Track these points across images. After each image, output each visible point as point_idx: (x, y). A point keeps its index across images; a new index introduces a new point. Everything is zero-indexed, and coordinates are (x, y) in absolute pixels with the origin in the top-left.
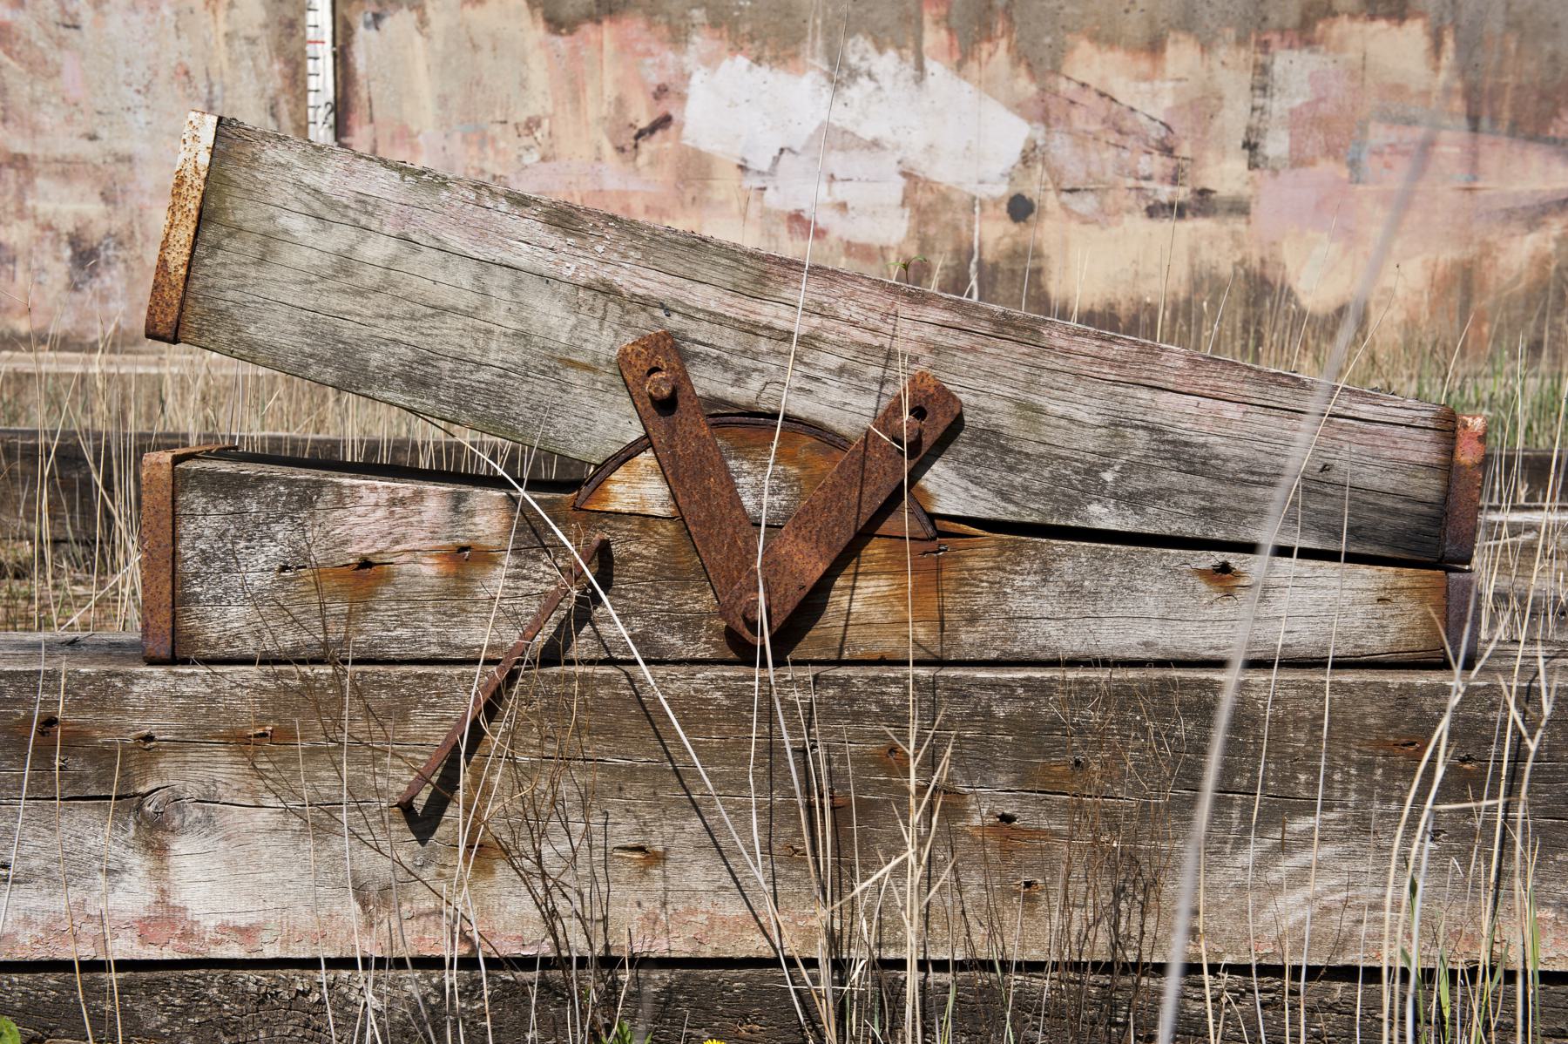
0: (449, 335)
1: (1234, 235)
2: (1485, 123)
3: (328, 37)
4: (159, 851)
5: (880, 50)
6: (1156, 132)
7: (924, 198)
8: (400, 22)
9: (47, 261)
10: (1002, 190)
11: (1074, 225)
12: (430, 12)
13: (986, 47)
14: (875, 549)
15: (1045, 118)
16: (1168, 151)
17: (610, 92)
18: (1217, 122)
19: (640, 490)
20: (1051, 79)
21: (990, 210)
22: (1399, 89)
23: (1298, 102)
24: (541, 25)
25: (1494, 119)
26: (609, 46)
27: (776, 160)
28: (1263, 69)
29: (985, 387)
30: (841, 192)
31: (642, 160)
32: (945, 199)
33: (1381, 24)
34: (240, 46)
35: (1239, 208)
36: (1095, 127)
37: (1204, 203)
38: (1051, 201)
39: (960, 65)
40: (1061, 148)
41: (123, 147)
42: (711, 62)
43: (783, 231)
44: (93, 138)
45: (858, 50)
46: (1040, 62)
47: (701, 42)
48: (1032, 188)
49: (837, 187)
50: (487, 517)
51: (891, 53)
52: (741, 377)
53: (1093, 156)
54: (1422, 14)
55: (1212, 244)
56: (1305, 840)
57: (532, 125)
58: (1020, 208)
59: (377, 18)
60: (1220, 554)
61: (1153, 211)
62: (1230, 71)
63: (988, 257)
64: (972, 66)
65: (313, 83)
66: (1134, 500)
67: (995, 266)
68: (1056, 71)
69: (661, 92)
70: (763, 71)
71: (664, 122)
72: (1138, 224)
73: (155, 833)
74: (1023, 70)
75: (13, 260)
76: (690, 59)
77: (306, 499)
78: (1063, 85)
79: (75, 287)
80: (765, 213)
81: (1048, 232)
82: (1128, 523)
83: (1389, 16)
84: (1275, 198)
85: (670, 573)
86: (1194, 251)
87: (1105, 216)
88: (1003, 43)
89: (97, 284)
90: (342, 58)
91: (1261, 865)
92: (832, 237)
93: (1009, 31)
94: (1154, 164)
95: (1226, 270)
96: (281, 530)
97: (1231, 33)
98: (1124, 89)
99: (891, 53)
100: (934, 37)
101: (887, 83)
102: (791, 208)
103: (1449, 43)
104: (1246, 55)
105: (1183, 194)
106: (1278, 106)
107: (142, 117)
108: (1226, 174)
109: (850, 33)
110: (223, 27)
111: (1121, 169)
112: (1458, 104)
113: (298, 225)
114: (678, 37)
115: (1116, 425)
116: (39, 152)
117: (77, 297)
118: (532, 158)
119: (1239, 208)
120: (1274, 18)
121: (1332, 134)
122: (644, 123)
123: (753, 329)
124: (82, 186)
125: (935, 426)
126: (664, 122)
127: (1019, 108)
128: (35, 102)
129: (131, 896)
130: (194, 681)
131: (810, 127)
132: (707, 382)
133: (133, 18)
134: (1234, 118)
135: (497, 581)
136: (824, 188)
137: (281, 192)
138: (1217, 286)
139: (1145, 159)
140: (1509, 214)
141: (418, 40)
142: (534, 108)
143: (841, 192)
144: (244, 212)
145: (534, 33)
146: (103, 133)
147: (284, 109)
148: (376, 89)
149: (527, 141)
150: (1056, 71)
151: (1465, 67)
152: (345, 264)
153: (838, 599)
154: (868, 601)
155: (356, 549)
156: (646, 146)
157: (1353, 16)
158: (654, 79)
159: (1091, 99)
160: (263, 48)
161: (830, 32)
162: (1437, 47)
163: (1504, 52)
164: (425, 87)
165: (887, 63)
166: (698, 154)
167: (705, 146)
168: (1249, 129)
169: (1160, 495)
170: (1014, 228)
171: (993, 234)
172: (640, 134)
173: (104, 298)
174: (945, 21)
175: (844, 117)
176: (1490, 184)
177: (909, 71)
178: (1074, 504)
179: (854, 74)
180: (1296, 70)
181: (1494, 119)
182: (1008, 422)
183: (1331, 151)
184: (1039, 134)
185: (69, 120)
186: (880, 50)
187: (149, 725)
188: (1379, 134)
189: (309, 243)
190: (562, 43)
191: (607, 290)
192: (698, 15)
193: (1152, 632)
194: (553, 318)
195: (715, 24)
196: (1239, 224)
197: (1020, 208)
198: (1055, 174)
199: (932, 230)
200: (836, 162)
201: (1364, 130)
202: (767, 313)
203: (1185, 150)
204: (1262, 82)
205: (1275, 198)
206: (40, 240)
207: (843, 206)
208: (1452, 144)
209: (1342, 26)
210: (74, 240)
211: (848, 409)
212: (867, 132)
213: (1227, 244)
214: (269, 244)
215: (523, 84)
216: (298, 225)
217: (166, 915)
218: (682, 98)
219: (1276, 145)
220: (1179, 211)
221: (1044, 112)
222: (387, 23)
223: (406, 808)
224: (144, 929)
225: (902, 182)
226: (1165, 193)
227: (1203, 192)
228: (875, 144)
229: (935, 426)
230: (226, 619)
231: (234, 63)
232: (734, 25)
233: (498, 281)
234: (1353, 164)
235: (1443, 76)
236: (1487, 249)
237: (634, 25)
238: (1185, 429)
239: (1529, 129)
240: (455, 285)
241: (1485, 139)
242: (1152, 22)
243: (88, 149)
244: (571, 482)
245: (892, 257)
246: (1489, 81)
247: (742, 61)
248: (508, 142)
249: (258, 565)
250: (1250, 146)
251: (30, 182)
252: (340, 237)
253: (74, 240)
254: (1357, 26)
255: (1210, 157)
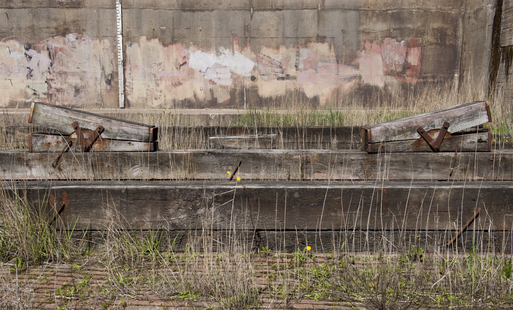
0: (56, 122)
1: (294, 83)
2: (340, 62)
3: (122, 49)
4: (31, 170)
5: (226, 49)
6: (278, 64)
7: (235, 77)
8: (135, 45)
9: (70, 91)
10: (250, 75)
11: (264, 81)
12: (141, 43)
13: (246, 48)
14: (97, 141)
15: (257, 61)
16: (281, 67)
17: (175, 57)
18: (290, 62)
19: (74, 136)
20: (258, 54)
21: (247, 79)
22: (323, 56)
23: (305, 58)
24: (162, 45)
25: (341, 61)
26: (174, 49)
27: (206, 70)
28: (298, 52)
29: (106, 126)
30: (219, 76)
31: (181, 70)
32: (239, 77)
33: (320, 44)
34: (105, 50)
35: (295, 78)
36: (267, 63)
37: (288, 77)
38: (259, 77)
39: (241, 52)
40: (261, 67)
41: (84, 70)
42: (194, 52)
43: (208, 83)
44: (78, 68)
45: (221, 49)
46: (256, 51)
47: (192, 48)
48: (256, 74)
49: (218, 75)
50: (60, 138)
51: (228, 49)
52: (83, 126)
53: (267, 69)
54: (327, 42)
55: (289, 84)
56: (136, 168)
57: (160, 64)
58: (253, 78)
59: (131, 44)
60: (129, 141)
61: (278, 79)
62: (292, 52)
63: (247, 88)
64: (243, 52)
65: (119, 57)
66: (121, 136)
67: (249, 89)
68: (259, 53)
69: (184, 57)
70: (204, 53)
71: (185, 63)
72: (276, 81)
73: (30, 168)
74: (253, 52)
75: (64, 91)
76: (190, 51)
77: (44, 137)
78: (261, 55)
79: (75, 96)
80: (205, 80)
81: (259, 83)
82: (120, 139)
83: (321, 42)
84: (300, 76)
85: (77, 144)
86: (286, 86)
87: (269, 80)
88: (249, 47)
89: (79, 95)
90: (124, 52)
91: (132, 170)
92: (218, 84)
93: (250, 45)
94: (279, 70)
95: (293, 90)
96: (41, 140)
97: (292, 45)
98: (272, 56)
99: (228, 49)
100: (236, 47)
101: (227, 55)
102: (210, 79)
103: (333, 47)
104: (295, 49)
105: (284, 75)
106: (301, 59)
107: (87, 64)
108: (292, 72)
109: (220, 46)
110: (102, 47)
111: (272, 71)
112: (335, 58)
113: (42, 112)
114: (188, 47)
115: (119, 130)
116: (69, 71)
117: (76, 98)
118: (160, 70)
119: (295, 78)
120: (300, 42)
121: (312, 64)
122: (181, 63)
123: (84, 121)
124: (76, 77)
125: (101, 130)
126: (185, 63)
127: (252, 59)
128: (68, 62)
129: (29, 174)
130: (33, 154)
131: (213, 63)
132: (80, 126)
133: (86, 46)
134: (293, 61)
135: (61, 145)
136: (216, 75)
137: (40, 109)
138: (291, 94)
139: (276, 69)
140: (345, 79)
141: (139, 48)
142: (161, 61)
143: (219, 76)
144: (37, 111)
145: (160, 47)
146: (80, 67)
147: (114, 62)
148: (131, 58)
149: (159, 67)
150: (259, 53)
151: (336, 52)
152: (46, 116)
153: (93, 146)
154: (96, 146)
155: (48, 142)
156: (182, 68)
157: (314, 42)
158: (183, 55)
159: (266, 58)
160: (110, 51)
161: (216, 46)
162: (330, 48)
163: (343, 49)
164: (140, 57)
165: (227, 51)
166: (192, 69)
167: (193, 67)
168: (296, 63)
169: (123, 136)
170: (252, 82)
171: (248, 83)
172: (181, 65)
173: (81, 98)
174: (238, 43)
175: (219, 62)
176: (341, 73)
177: (231, 53)
178: (115, 137)
179: (221, 54)
180: (304, 52)
181: (341, 61)
182: (109, 129)
183: (311, 67)
184: (256, 65)
185: (74, 65)
186: (226, 49)
187: (30, 158)
188: (320, 64)
189: (43, 114)
190: (166, 49)
191: (71, 118)
192: (191, 43)
193: (123, 149)
194: (66, 121)
195: (194, 45)
196: (295, 81)
197: (253, 78)
198: (260, 72)
199: (236, 83)
200: (218, 70)
201: (317, 63)
202: (85, 120)
203: (284, 67)
204: (298, 55)
205: (300, 76)
206: (69, 87)
207: (220, 78)
208: (333, 66)
209: (313, 44)
210: (75, 87)
211: (93, 128)
212: (224, 64)
213: (292, 85)
214: (39, 114)
215: (158, 57)
216: (42, 112)
217: (32, 175)
218: (188, 58)
219: (301, 66)
220: (283, 78)
221: (257, 60)
222: (133, 46)
223: (53, 165)
224: (30, 177)
225: (231, 74)
226: (280, 75)
227: (288, 75)
228: (225, 67)
229: (101, 130)
230: (36, 149)
231: (104, 53)
232: (198, 45)
233: (60, 117)
234: (316, 70)
235: (332, 53)
236: (341, 86)
237: (179, 45)
238: (125, 130)
239: (348, 63)
240: (56, 118)
241: (340, 65)
242: (277, 44)
243: (78, 70)
244: (67, 136)
245: (229, 88)
246: (340, 54)
247: (200, 51)
248: (156, 67)
249: (39, 144)
250: (296, 66)
251: (67, 77)
252: (46, 113)
253: (75, 87)
254: (315, 44)
255: (289, 68)
